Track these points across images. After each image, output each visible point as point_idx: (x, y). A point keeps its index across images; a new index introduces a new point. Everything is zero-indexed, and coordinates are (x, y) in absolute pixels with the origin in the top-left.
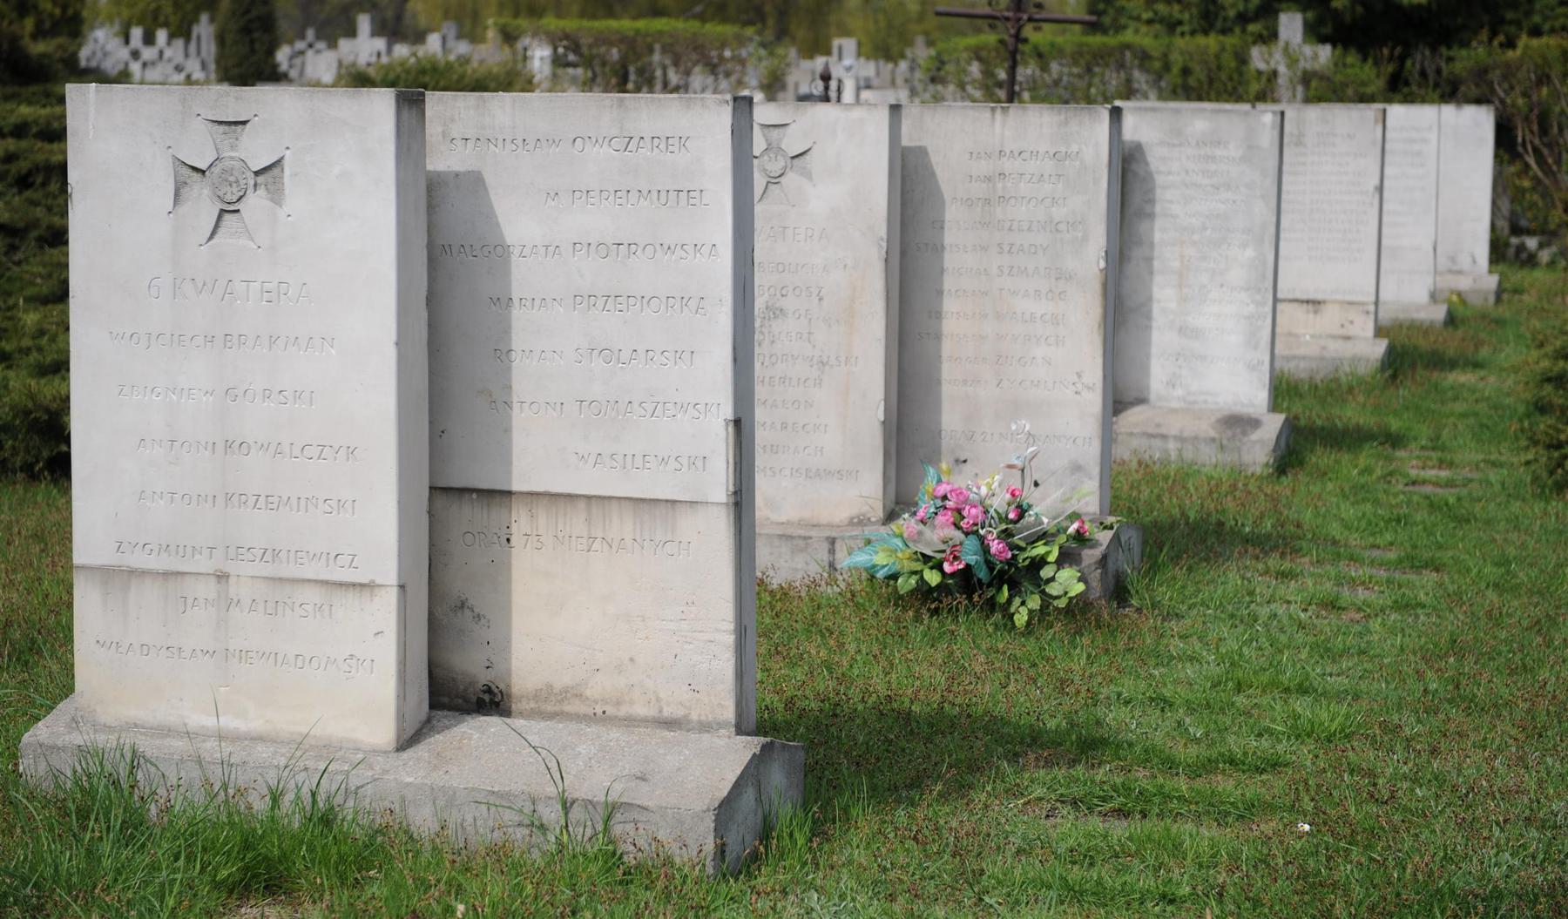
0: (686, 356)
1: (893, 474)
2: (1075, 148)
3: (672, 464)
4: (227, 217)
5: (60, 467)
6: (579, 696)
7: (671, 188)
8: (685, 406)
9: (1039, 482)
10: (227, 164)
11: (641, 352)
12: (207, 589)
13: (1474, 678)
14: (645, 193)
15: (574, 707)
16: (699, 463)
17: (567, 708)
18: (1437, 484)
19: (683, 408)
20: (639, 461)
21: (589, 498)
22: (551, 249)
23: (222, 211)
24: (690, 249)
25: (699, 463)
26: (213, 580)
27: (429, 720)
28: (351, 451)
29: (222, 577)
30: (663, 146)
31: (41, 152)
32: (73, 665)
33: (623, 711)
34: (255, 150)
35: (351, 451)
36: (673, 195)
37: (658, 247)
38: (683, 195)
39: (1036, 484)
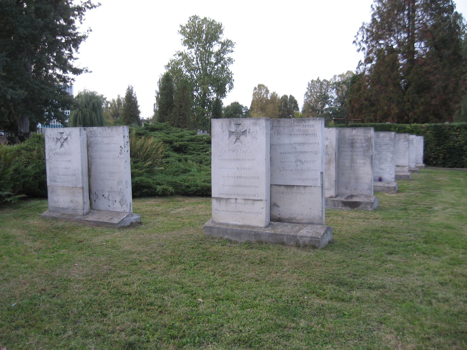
1: (336, 189)
2: (367, 135)
4: (238, 140)
6: (295, 219)
10: (237, 131)
13: (38, 332)
15: (294, 221)
17: (293, 221)
18: (397, 197)
19: (313, 170)
20: (305, 180)
21: (297, 186)
23: (237, 139)
26: (235, 199)
28: (258, 178)
29: (236, 199)
31: (208, 157)
33: (303, 221)
34: (241, 129)
35: (258, 178)
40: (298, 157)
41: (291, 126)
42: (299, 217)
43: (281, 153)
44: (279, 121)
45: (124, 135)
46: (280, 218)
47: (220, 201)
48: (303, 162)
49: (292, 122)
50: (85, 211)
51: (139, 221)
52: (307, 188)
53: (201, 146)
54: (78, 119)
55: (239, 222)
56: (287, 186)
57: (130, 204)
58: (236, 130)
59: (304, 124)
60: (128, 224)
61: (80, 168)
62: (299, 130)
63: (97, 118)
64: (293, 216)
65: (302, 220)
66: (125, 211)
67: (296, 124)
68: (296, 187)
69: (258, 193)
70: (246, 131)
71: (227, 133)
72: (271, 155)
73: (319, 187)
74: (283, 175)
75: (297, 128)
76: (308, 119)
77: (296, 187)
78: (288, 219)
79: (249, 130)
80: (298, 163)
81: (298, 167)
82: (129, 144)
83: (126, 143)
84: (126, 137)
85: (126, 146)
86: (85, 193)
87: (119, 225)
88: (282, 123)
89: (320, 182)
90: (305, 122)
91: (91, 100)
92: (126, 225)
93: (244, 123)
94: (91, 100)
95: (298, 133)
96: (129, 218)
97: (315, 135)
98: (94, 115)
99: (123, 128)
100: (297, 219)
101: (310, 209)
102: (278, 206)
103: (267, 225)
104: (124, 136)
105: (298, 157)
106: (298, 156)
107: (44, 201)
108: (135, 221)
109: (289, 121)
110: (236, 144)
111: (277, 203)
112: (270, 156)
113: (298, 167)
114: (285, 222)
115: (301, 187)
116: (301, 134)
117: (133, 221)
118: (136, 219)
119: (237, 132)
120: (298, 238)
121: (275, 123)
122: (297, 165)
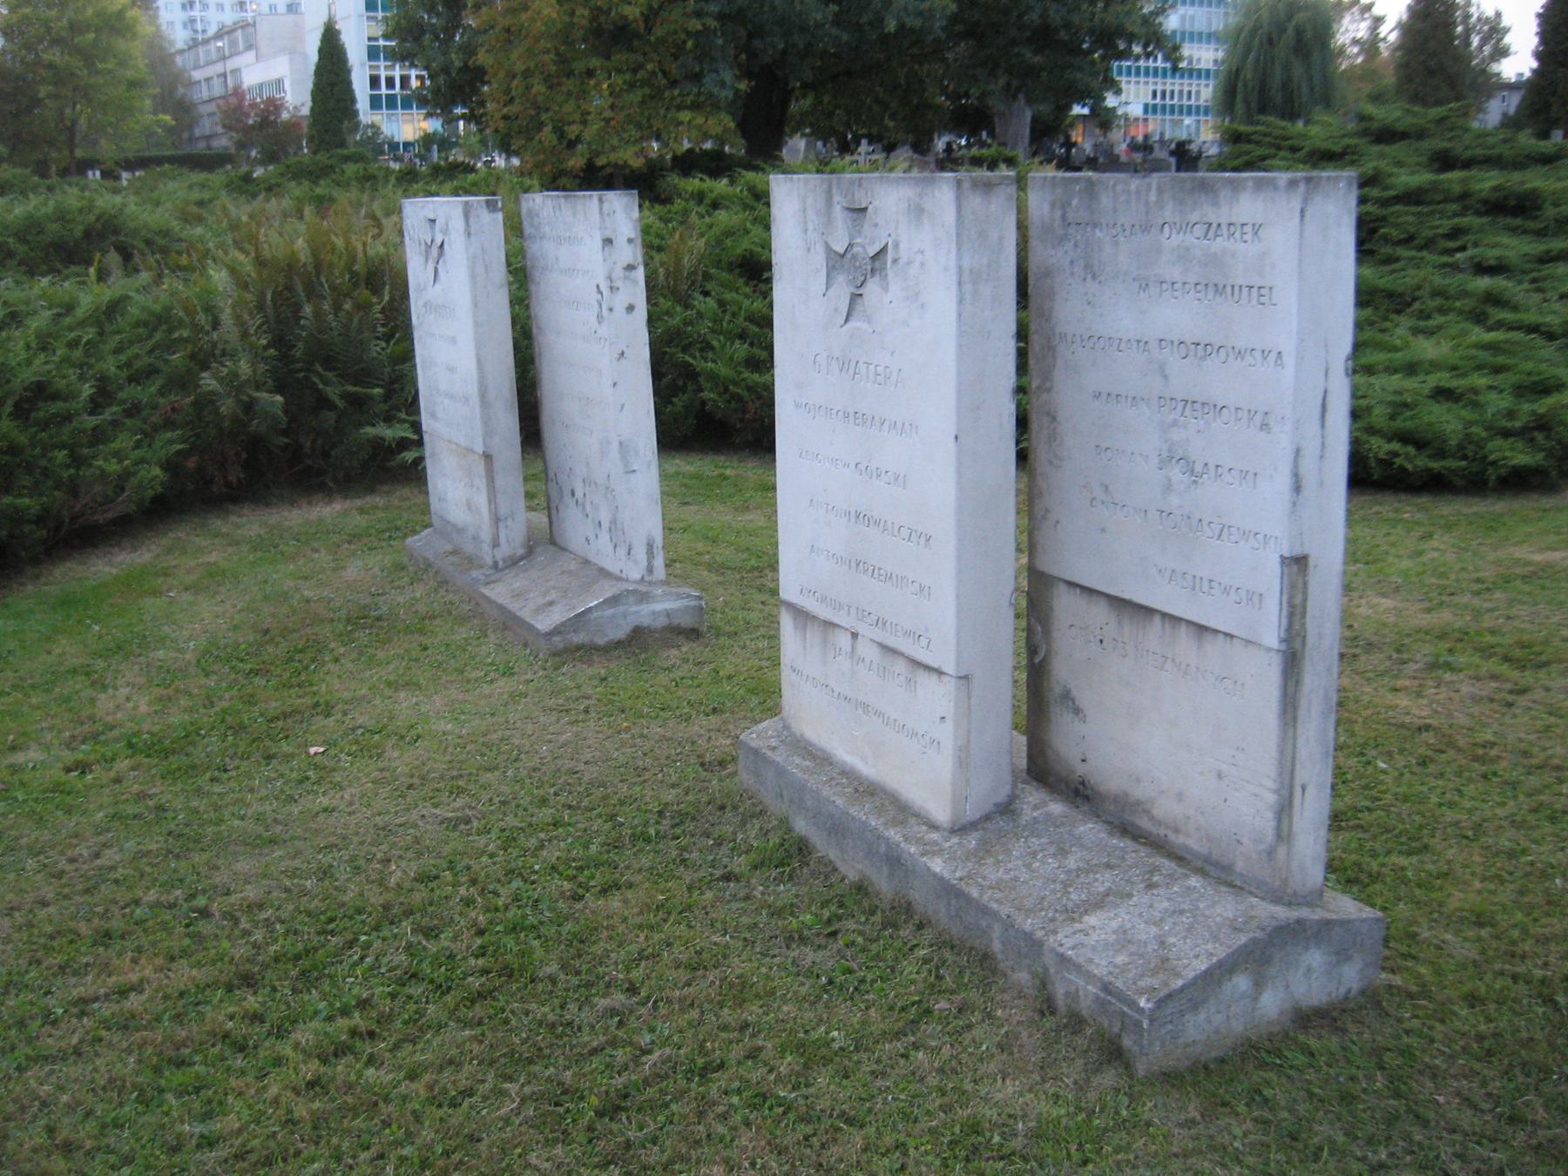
0: (1250, 477)
3: (1233, 596)
5: (770, 448)
6: (1147, 812)
7: (1245, 283)
8: (605, 312)
9: (1298, 551)
11: (1211, 467)
12: (844, 640)
14: (1220, 286)
16: (1256, 599)
21: (1164, 615)
22: (1142, 344)
24: (1258, 354)
25: (1256, 599)
26: (849, 635)
27: (1007, 809)
30: (1237, 235)
32: (777, 562)
36: (1245, 290)
37: (1230, 350)
38: (1254, 291)
39: (611, 310)
40: (1176, 435)
41: (1146, 229)
42: (1166, 808)
43: (1098, 395)
44: (1091, 189)
45: (608, 234)
46: (1083, 783)
47: (805, 628)
48: (1198, 468)
49: (1153, 197)
50: (504, 551)
51: (687, 621)
52: (1215, 646)
53: (1446, 225)
54: (1240, 84)
55: (864, 759)
56: (1120, 604)
57: (650, 547)
58: (850, 245)
59: (1212, 215)
60: (620, 633)
61: (475, 376)
62: (1184, 255)
63: (1310, 79)
64: (1138, 793)
65: (1177, 831)
66: (624, 576)
67: (1169, 212)
68: (1157, 620)
69: (927, 629)
70: (883, 250)
71: (819, 258)
72: (1019, 405)
73: (1269, 650)
74: (1103, 530)
75: (1176, 239)
76: (1231, 182)
77: (1157, 620)
78: (1116, 800)
79: (896, 245)
80: (1176, 473)
81: (1174, 500)
82: (640, 274)
83: (618, 272)
84: (621, 241)
85: (618, 284)
86: (499, 482)
87: (556, 639)
88: (1105, 200)
89: (1274, 619)
90: (1216, 204)
91: (1290, 17)
92: (600, 641)
93: (876, 203)
94: (1290, 17)
95: (1175, 273)
96: (621, 609)
97: (1261, 293)
98: (1298, 70)
99: (601, 200)
100: (1155, 812)
101: (1220, 776)
102: (1077, 711)
103: (971, 812)
104: (608, 241)
105: (1176, 435)
106: (1175, 423)
107: (401, 495)
108: (661, 622)
109: (1138, 192)
110: (851, 324)
111: (1075, 693)
112: (1012, 407)
113: (1174, 500)
114: (1097, 815)
115: (1183, 628)
116: (1192, 279)
117: (646, 621)
118: (668, 614)
119: (854, 257)
120: (1049, 959)
121: (1075, 202)
122: (1168, 488)
